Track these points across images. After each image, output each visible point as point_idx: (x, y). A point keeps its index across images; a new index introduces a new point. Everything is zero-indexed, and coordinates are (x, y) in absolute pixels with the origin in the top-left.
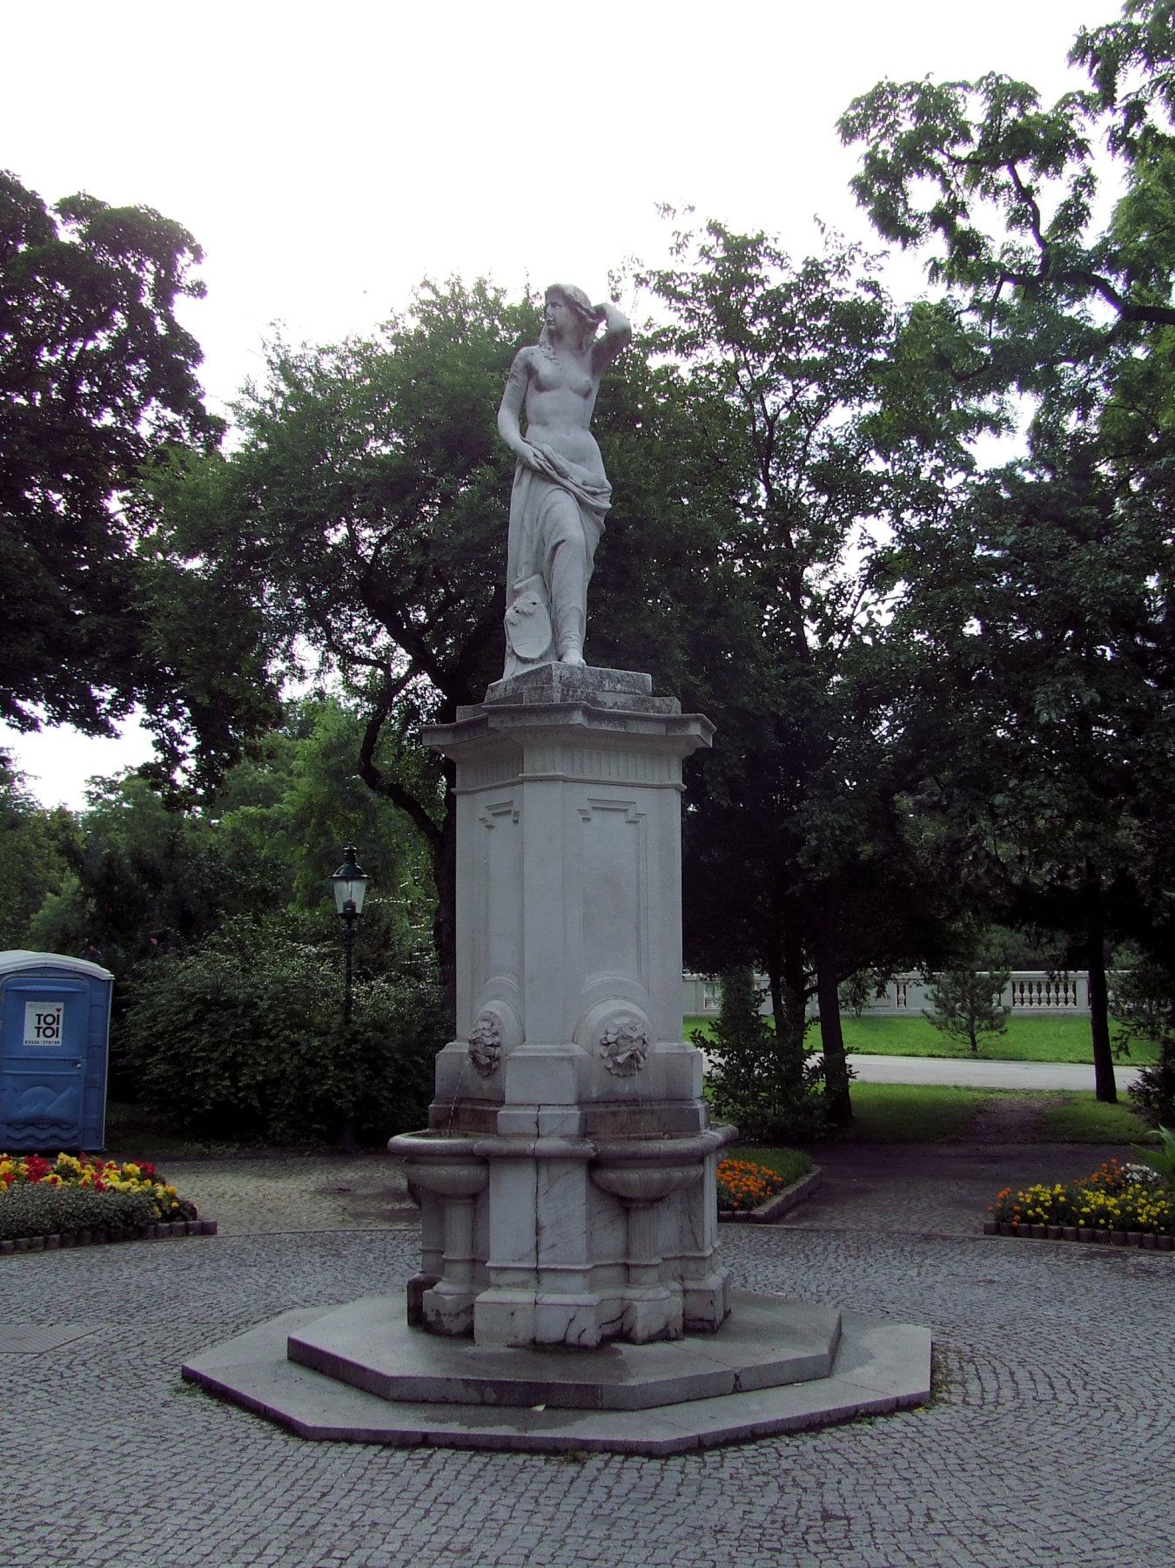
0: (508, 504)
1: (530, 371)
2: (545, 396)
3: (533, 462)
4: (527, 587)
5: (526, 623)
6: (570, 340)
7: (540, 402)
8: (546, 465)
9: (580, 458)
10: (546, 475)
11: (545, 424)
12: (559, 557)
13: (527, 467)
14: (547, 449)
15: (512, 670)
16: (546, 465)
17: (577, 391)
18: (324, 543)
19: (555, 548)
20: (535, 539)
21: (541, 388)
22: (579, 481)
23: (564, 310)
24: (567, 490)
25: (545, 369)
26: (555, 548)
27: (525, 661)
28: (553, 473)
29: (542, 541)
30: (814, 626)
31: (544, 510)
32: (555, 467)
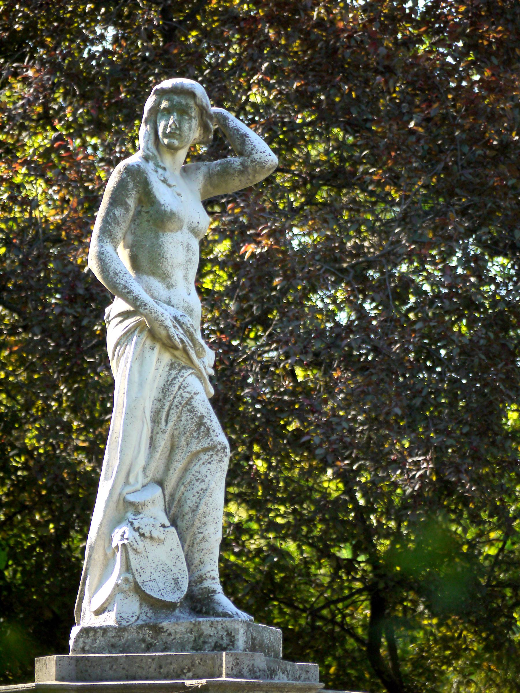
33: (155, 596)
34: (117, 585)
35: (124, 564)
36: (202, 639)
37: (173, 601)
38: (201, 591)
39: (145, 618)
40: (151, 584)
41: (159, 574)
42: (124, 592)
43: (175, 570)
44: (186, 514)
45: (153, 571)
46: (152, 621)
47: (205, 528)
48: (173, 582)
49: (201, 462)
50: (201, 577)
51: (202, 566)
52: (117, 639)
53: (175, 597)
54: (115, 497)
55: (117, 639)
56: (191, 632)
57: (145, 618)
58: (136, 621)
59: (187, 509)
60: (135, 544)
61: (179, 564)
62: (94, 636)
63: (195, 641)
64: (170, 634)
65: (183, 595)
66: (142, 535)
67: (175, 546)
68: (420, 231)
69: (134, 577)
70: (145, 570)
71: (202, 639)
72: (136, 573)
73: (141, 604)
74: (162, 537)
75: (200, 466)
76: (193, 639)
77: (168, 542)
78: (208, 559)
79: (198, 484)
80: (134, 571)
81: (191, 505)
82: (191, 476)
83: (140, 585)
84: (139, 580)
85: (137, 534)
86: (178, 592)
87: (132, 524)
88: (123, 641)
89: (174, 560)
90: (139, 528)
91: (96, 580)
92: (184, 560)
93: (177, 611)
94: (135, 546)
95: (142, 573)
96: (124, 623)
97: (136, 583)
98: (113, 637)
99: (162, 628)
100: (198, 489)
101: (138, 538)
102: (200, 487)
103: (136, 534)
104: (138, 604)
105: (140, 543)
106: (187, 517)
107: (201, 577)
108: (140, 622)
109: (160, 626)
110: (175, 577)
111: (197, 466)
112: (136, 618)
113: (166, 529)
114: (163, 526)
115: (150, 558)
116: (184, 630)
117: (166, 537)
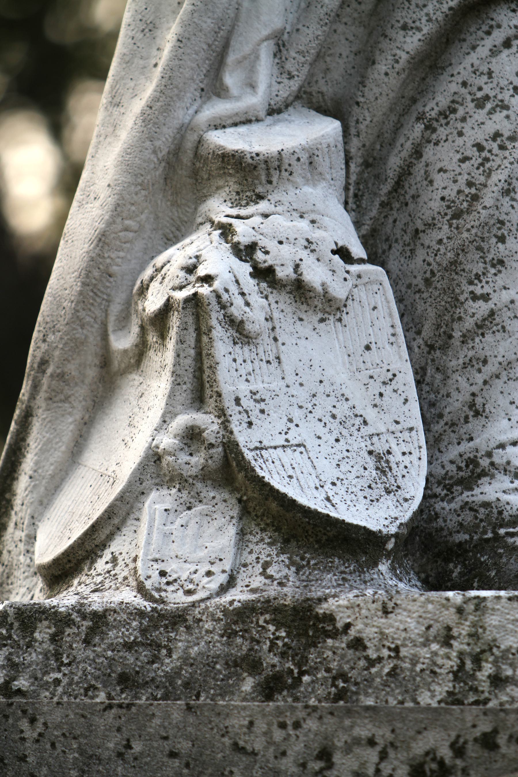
33: (303, 500)
34: (154, 457)
35: (188, 377)
36: (488, 669)
37: (373, 526)
38: (468, 517)
39: (258, 582)
40: (287, 457)
41: (321, 430)
42: (176, 480)
43: (378, 423)
44: (431, 225)
45: (297, 414)
46: (291, 593)
47: (500, 281)
48: (371, 462)
49: (498, 36)
50: (473, 462)
51: (474, 424)
52: (145, 654)
53: (381, 516)
54: (164, 142)
55: (145, 654)
56: (447, 638)
57: (258, 582)
58: (223, 589)
59: (432, 204)
60: (239, 301)
61: (392, 401)
62: (54, 638)
63: (459, 674)
64: (358, 644)
65: (406, 514)
66: (264, 274)
67: (382, 336)
68: (318, 660)
69: (225, 424)
70: (270, 406)
71: (488, 669)
72: (232, 409)
73: (242, 533)
74: (339, 290)
75: (494, 52)
76: (453, 663)
77: (354, 315)
78: (503, 401)
79: (481, 115)
80: (228, 403)
81: (451, 193)
82: (454, 87)
83: (249, 455)
84: (244, 438)
85: (246, 268)
86: (389, 501)
87: (226, 231)
88: (169, 664)
89: (376, 387)
90: (252, 247)
91: (59, 453)
92: (413, 393)
93: (384, 567)
94: (238, 308)
95: (255, 414)
96: (176, 599)
97: (231, 447)
98: (129, 646)
99: (330, 618)
100: (480, 136)
101: (250, 284)
102: (490, 128)
103: (244, 269)
104: (232, 531)
105: (256, 300)
106: (430, 238)
107: (473, 462)
108: (238, 596)
109: (322, 609)
110: (380, 447)
111: (483, 51)
112: (222, 578)
113: (354, 268)
114: (343, 253)
115: (288, 366)
116: (416, 630)
117: (350, 297)
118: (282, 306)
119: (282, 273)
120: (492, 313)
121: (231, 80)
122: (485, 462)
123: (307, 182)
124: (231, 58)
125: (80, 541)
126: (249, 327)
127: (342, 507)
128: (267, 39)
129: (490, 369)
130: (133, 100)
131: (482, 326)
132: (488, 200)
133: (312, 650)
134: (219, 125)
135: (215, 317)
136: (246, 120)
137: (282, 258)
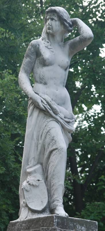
0: (25, 131)
1: (37, 53)
2: (45, 69)
3: (41, 104)
4: (35, 171)
5: (35, 191)
6: (58, 38)
7: (41, 71)
8: (48, 107)
9: (62, 103)
10: (47, 112)
11: (45, 84)
12: (53, 158)
13: (36, 106)
14: (49, 99)
15: (24, 215)
16: (48, 107)
17: (62, 67)
18: (101, 58)
19: (51, 152)
20: (40, 147)
21: (44, 63)
22: (62, 116)
23: (58, 23)
24: (57, 121)
25: (46, 54)
26: (51, 152)
27: (34, 212)
28: (51, 112)
29: (44, 148)
30: (95, 142)
31: (45, 131)
32: (52, 108)
47: (54, 181)
94: (26, 188)
118: (32, 187)
119: (31, 184)
120: (54, 184)
121: (29, 163)
122: (54, 200)
123: (35, 173)
124: (29, 161)
125: (21, 62)
126: (28, 190)
127: (64, 214)
128: (32, 158)
129: (54, 190)
130: (34, 71)
131: (53, 186)
132: (52, 172)
133: (12, 189)
134: (28, 168)
135: (24, 190)
136: (31, 167)
137: (31, 182)
